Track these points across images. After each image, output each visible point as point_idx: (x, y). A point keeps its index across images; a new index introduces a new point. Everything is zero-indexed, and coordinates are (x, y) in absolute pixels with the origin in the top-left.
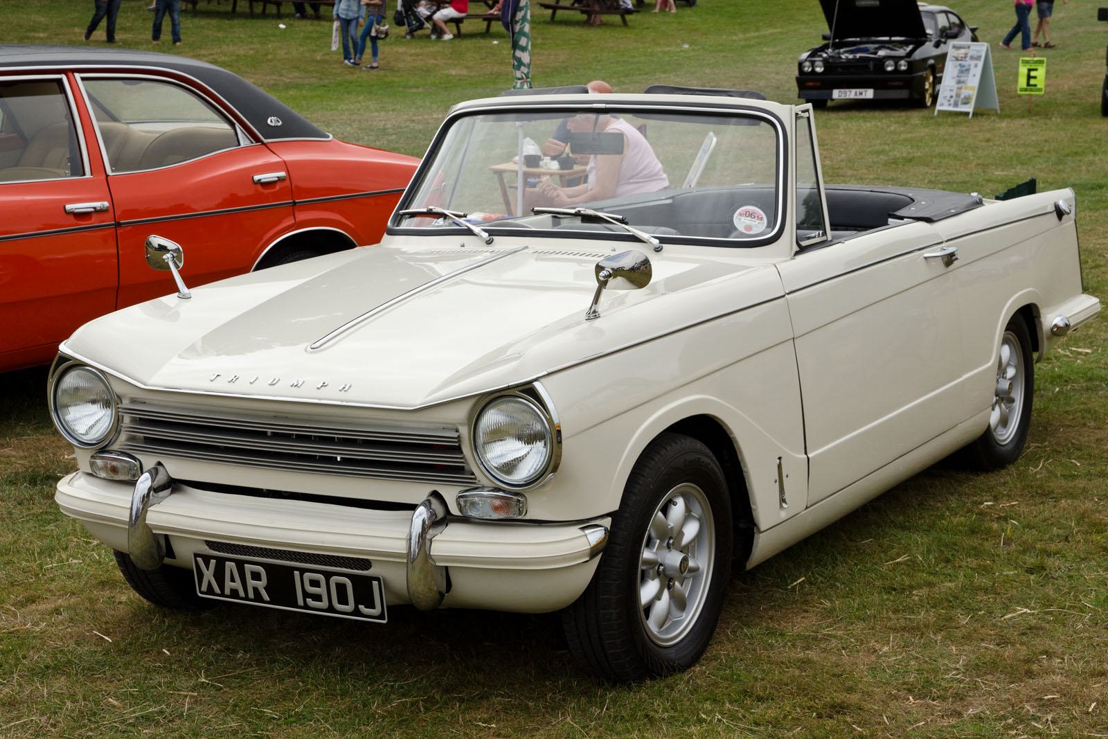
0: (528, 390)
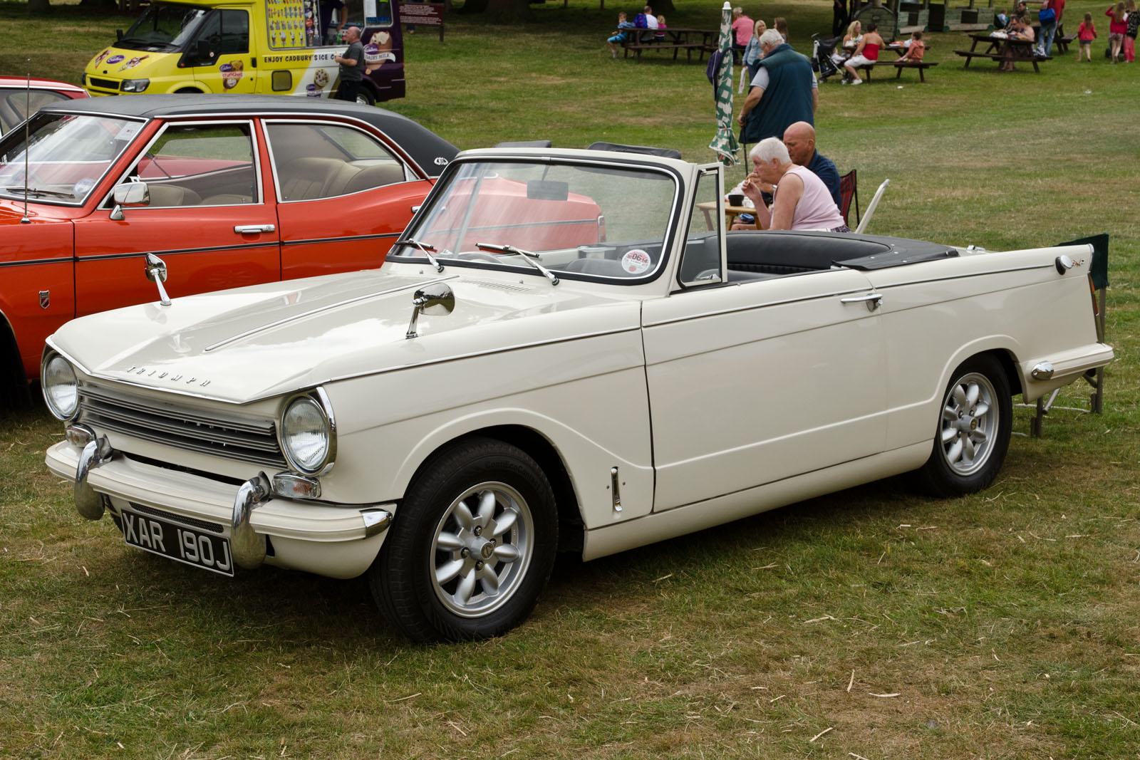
0: (310, 394)
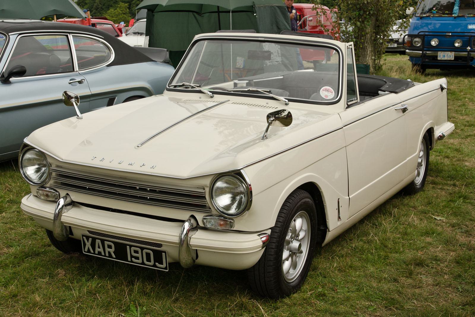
0: (237, 175)
